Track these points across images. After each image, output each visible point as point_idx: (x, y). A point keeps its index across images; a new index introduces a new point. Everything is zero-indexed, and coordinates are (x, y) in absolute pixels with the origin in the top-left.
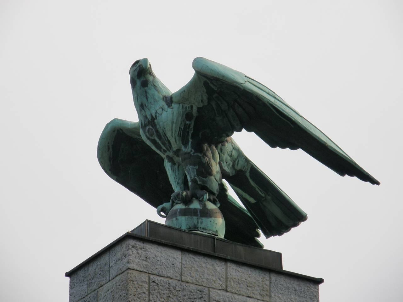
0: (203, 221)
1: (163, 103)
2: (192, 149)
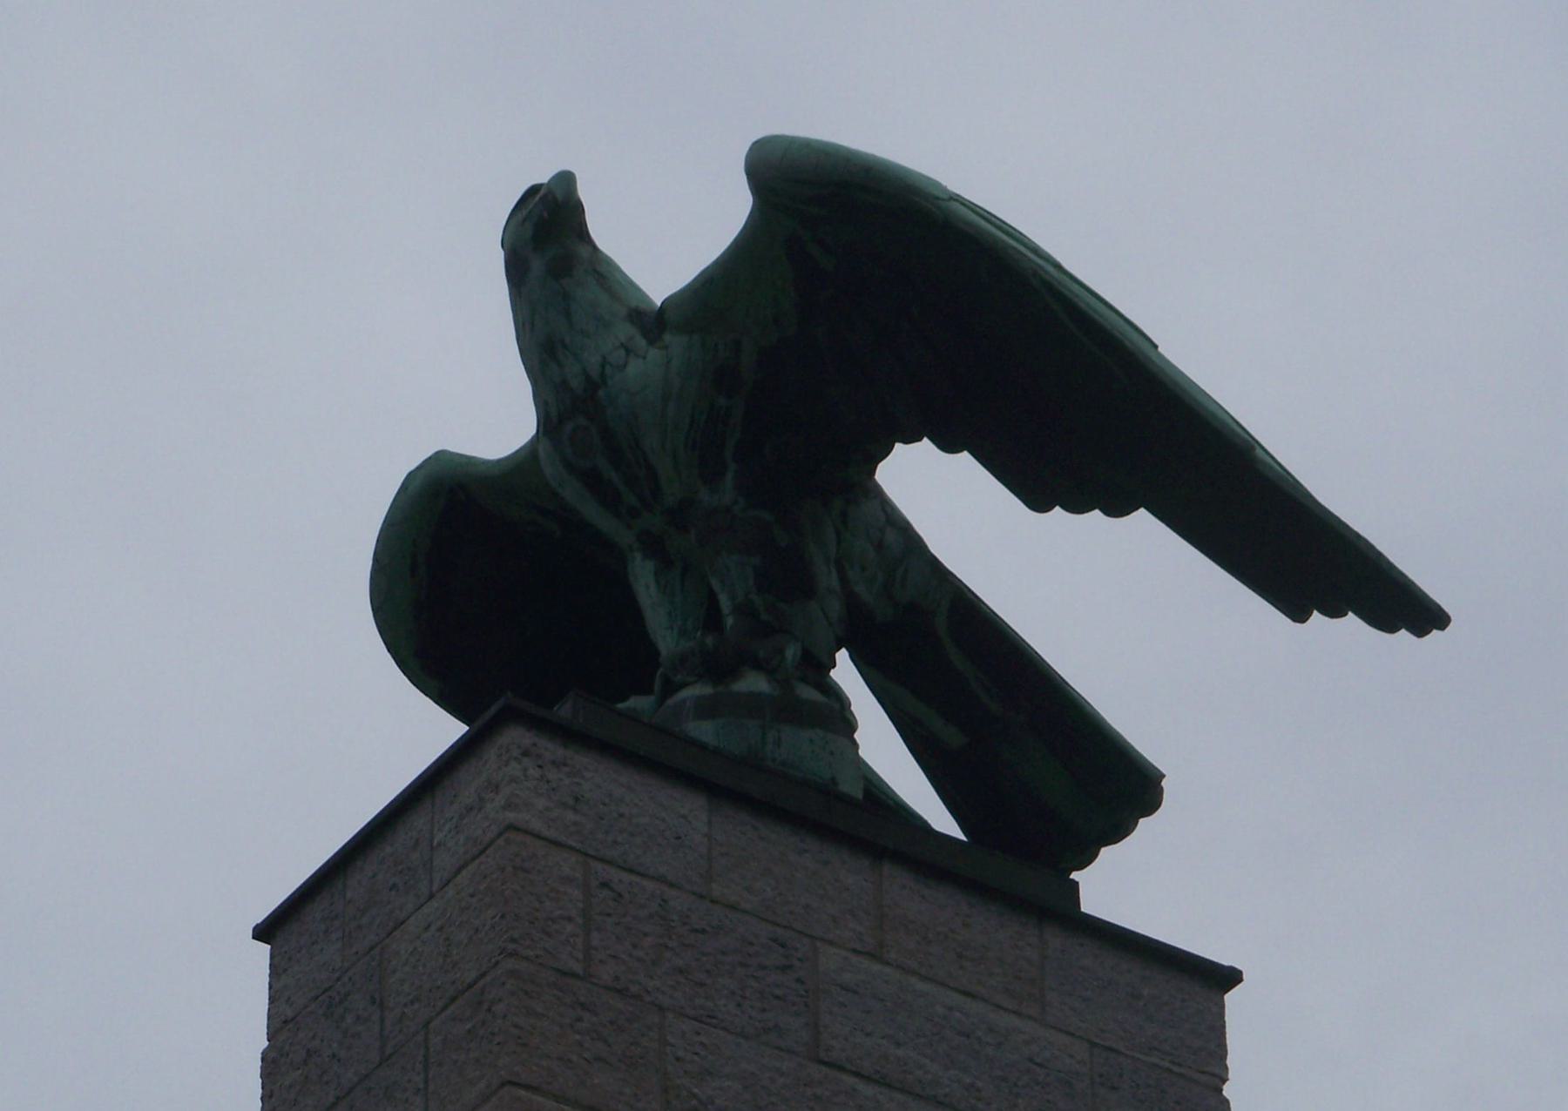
1: (625, 331)
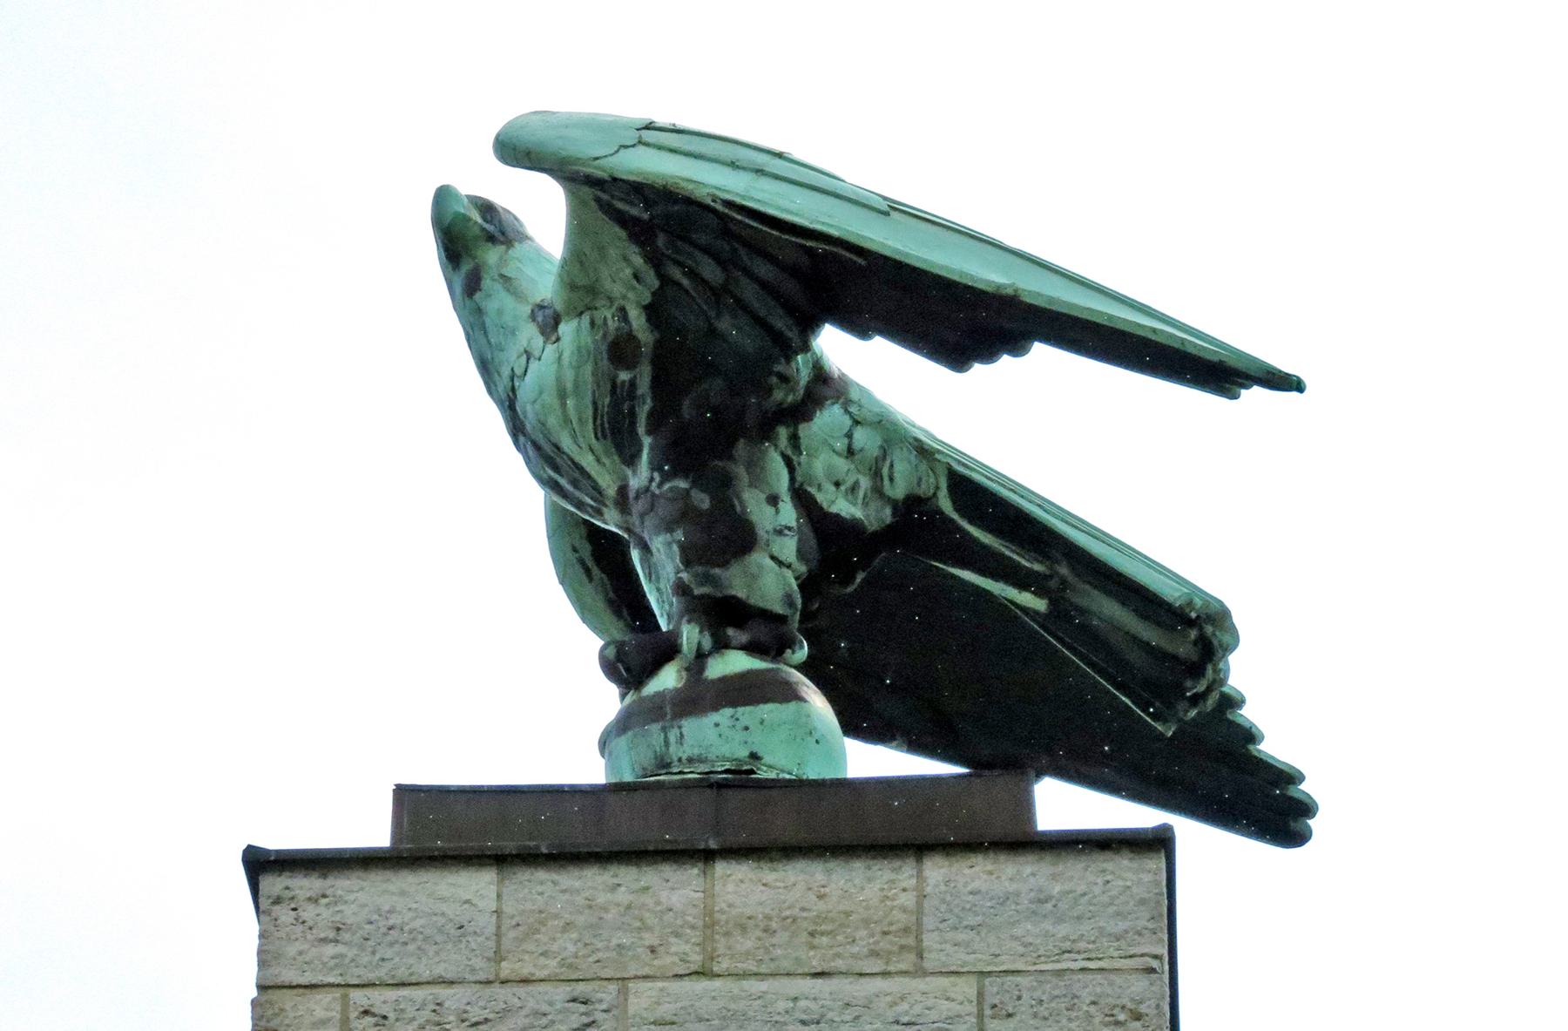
1: (529, 334)
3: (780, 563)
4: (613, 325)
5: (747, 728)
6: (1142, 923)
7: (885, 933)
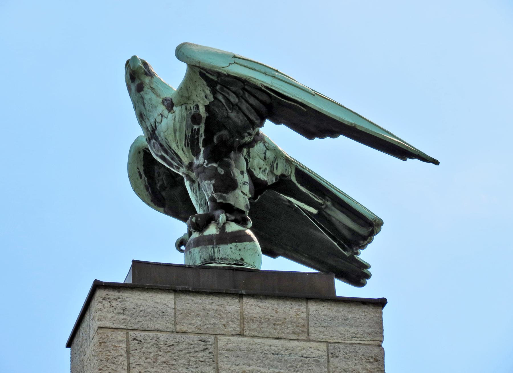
0: (220, 249)
1: (162, 109)
2: (205, 159)
3: (244, 194)
4: (193, 110)
5: (240, 250)
6: (377, 330)
7: (297, 326)
